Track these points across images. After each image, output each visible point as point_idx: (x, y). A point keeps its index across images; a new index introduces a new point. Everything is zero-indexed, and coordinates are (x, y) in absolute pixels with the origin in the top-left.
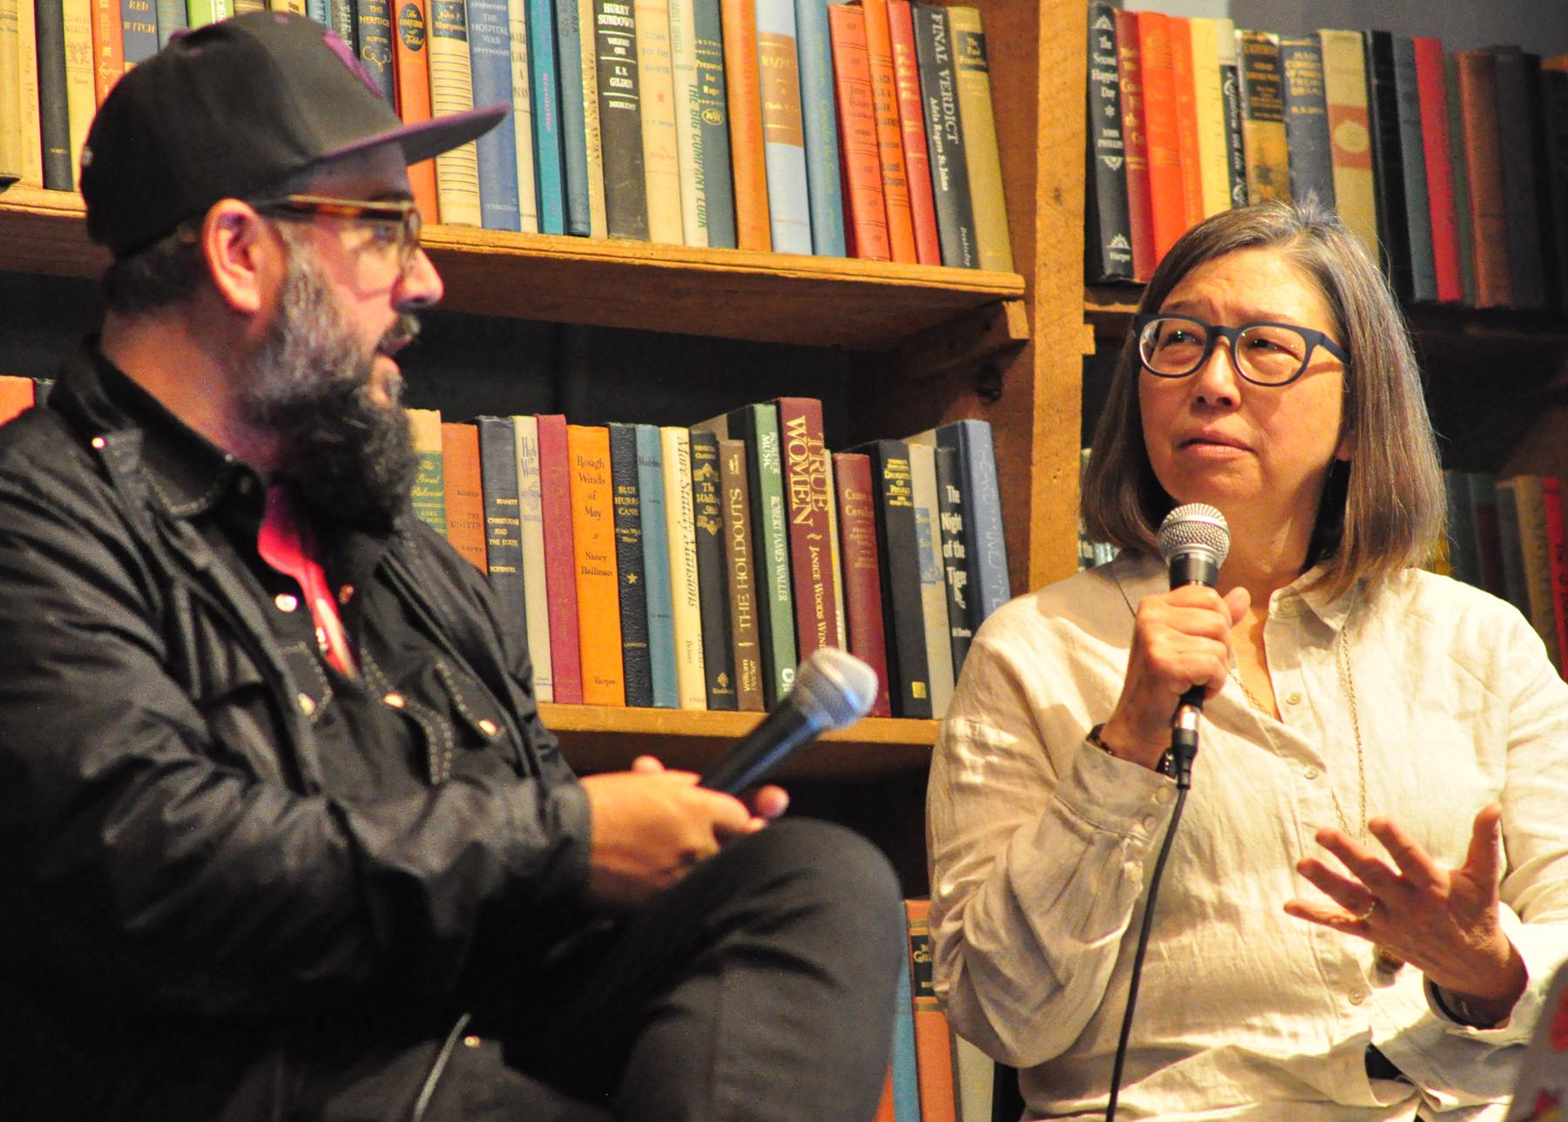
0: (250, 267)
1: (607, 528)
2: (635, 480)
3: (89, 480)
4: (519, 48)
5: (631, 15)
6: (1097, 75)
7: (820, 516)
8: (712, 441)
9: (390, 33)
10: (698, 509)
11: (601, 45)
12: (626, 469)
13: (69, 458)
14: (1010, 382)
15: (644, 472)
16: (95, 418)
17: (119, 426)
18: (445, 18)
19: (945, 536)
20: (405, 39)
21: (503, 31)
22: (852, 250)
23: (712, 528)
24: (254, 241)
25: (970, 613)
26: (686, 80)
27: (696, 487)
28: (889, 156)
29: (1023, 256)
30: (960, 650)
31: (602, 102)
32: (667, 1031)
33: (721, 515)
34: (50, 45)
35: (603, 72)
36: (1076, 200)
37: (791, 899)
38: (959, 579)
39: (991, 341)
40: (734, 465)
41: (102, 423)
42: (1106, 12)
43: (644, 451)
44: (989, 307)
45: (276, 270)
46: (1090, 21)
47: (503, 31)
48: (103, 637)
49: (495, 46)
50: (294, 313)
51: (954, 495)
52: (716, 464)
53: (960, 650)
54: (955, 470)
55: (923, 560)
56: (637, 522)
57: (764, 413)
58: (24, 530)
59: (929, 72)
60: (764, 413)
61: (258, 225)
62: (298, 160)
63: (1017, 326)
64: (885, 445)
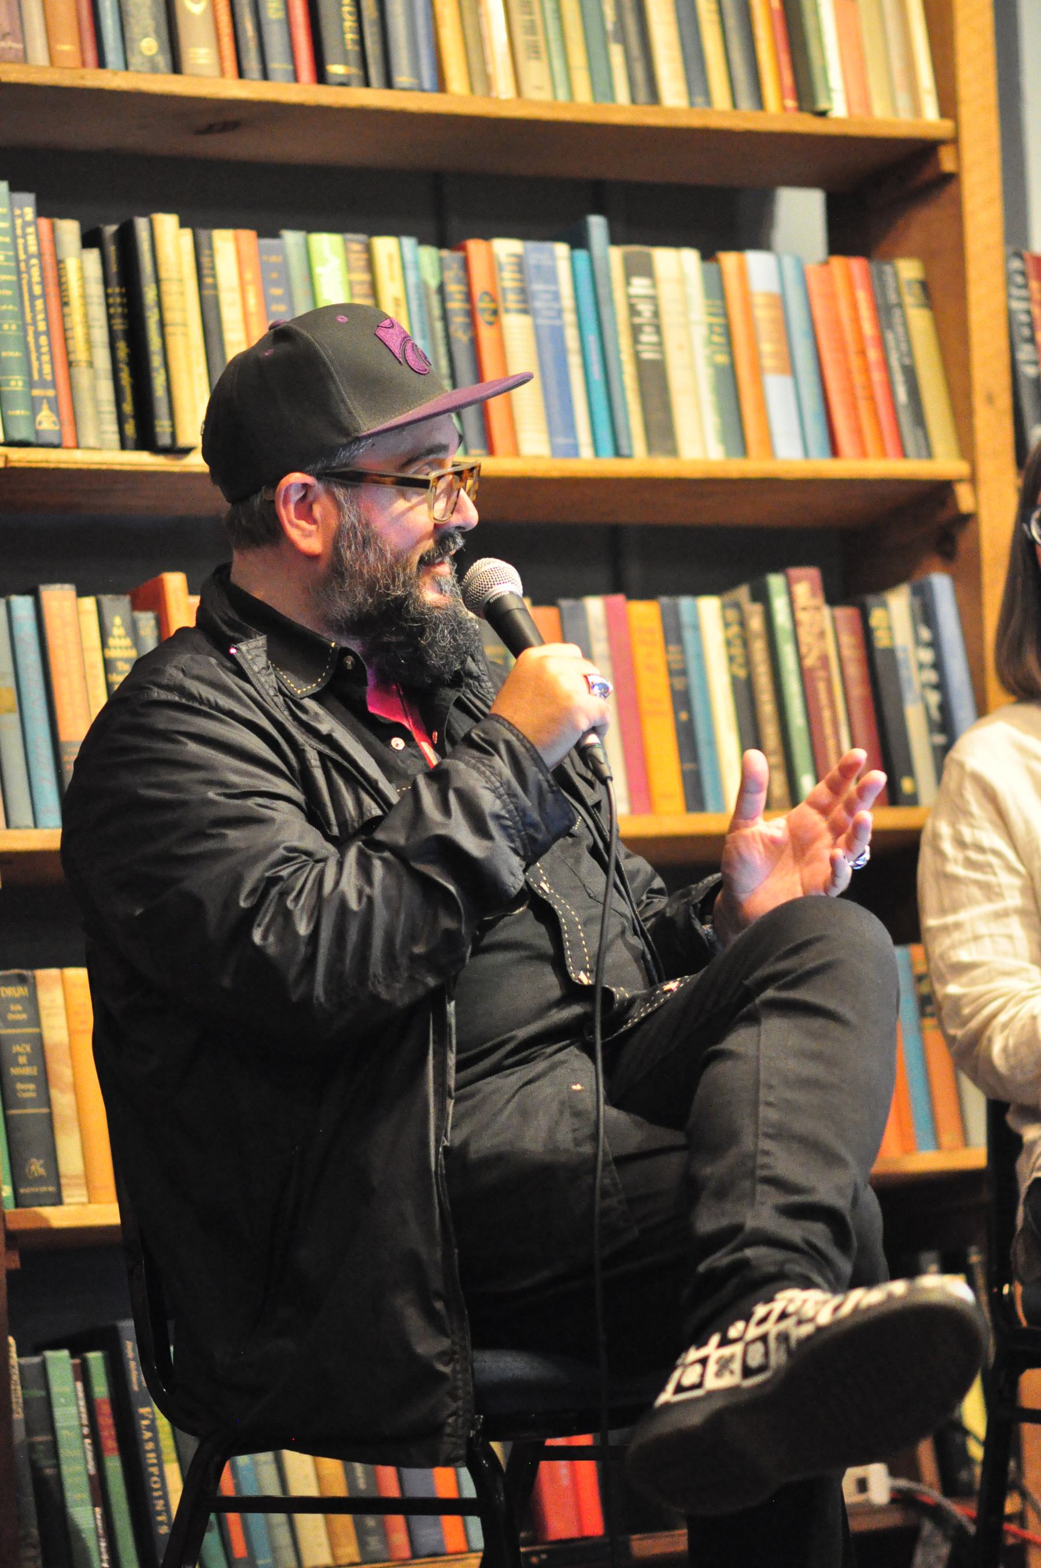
0: (313, 521)
1: (661, 679)
2: (679, 640)
3: (231, 680)
4: (569, 318)
5: (654, 285)
6: (1016, 305)
7: (824, 659)
8: (737, 606)
9: (471, 314)
10: (731, 659)
11: (633, 311)
12: (673, 632)
13: (212, 665)
14: (963, 544)
15: (688, 635)
16: (230, 633)
17: (249, 637)
18: (512, 300)
19: (921, 666)
20: (483, 318)
21: (555, 305)
22: (835, 451)
23: (742, 673)
24: (316, 499)
25: (945, 727)
26: (699, 333)
27: (729, 643)
28: (858, 379)
29: (967, 447)
30: (941, 753)
31: (637, 355)
32: (719, 1070)
33: (748, 663)
34: (213, 340)
35: (636, 331)
36: (1004, 401)
37: (809, 960)
38: (934, 698)
39: (944, 516)
40: (756, 623)
41: (237, 635)
42: (1019, 255)
43: (686, 617)
44: (940, 491)
45: (333, 523)
46: (1007, 261)
47: (555, 305)
48: (251, 802)
49: (551, 318)
50: (348, 555)
51: (925, 634)
52: (743, 624)
53: (941, 753)
54: (926, 614)
55: (905, 686)
56: (683, 672)
57: (776, 582)
58: (182, 728)
59: (885, 312)
60: (776, 582)
61: (318, 487)
62: (344, 441)
63: (965, 499)
64: (870, 599)
